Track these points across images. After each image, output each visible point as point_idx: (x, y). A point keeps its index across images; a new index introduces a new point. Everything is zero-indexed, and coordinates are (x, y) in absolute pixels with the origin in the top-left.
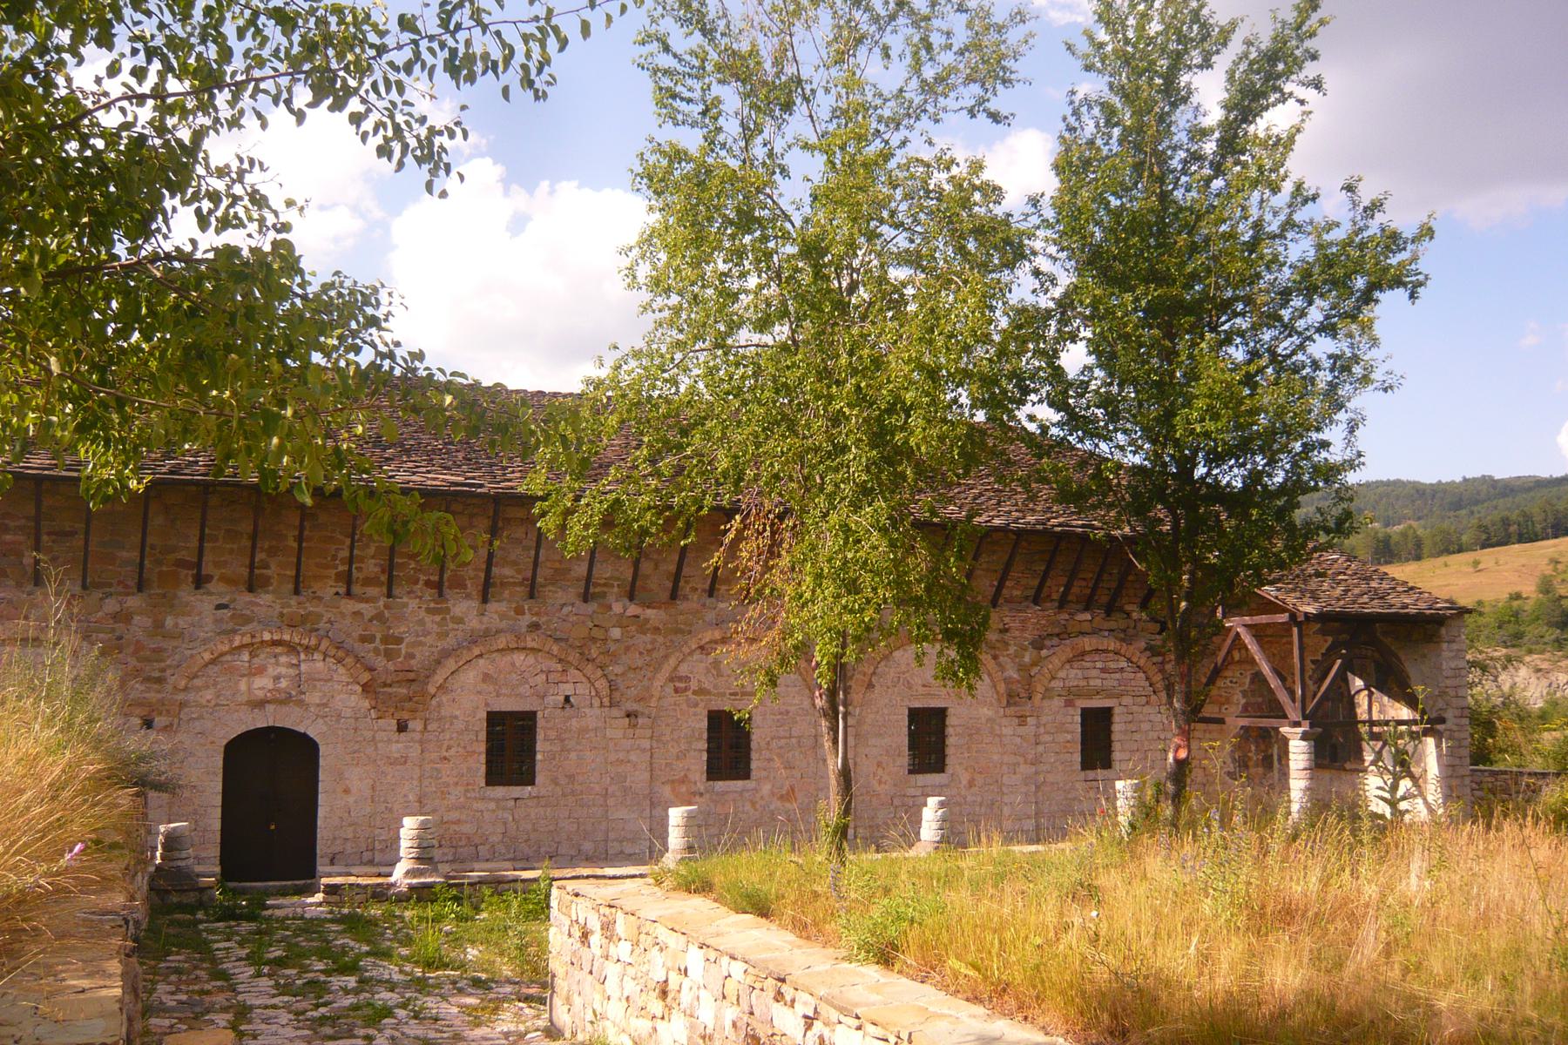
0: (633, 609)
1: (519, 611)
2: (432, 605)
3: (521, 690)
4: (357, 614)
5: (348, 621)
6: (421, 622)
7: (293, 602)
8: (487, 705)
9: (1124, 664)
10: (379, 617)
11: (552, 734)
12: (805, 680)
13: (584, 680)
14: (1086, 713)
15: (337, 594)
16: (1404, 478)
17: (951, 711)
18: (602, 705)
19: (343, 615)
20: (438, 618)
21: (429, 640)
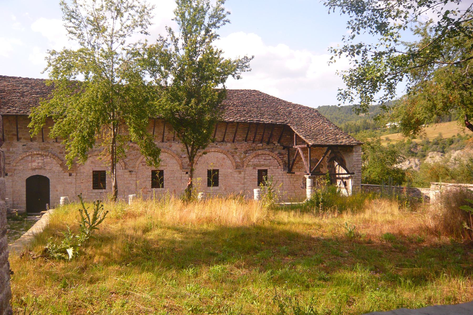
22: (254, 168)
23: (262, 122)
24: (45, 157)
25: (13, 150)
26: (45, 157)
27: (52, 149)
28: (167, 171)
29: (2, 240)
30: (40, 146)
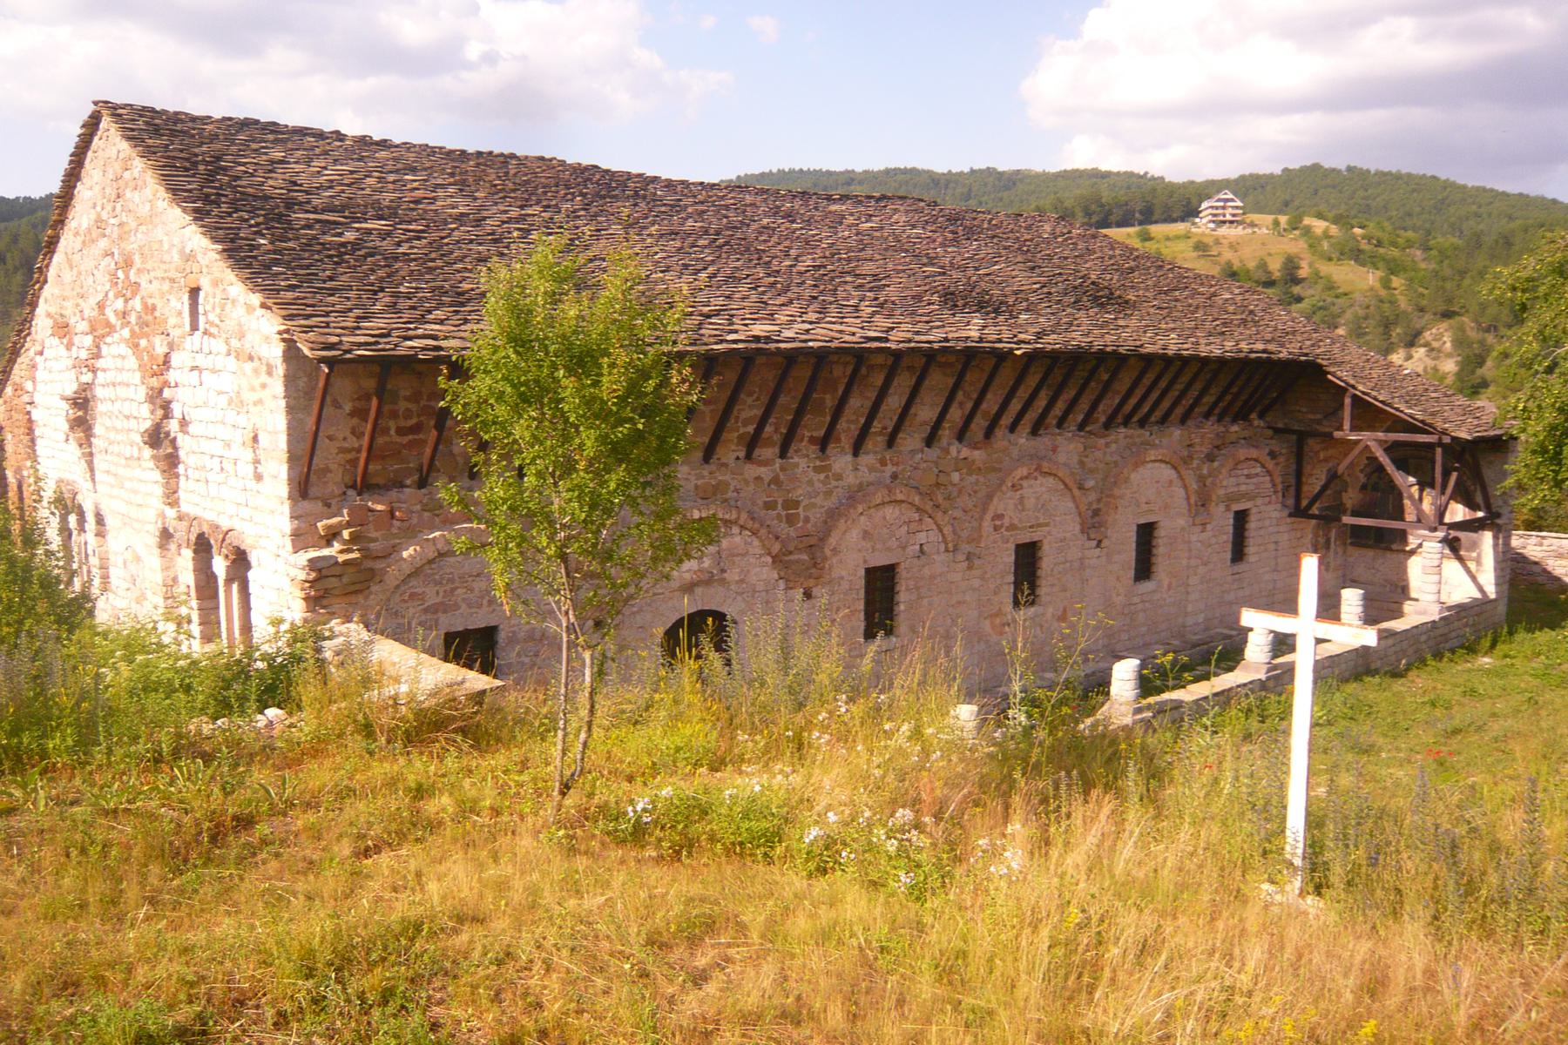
0: (965, 452)
1: (883, 463)
2: (818, 463)
3: (889, 544)
4: (758, 479)
5: (751, 487)
6: (810, 482)
7: (706, 473)
8: (865, 562)
9: (1259, 470)
10: (775, 480)
11: (911, 583)
12: (1077, 507)
13: (934, 527)
14: (1237, 513)
15: (738, 458)
16: (920, 167)
17: (1161, 524)
18: (947, 550)
19: (747, 482)
20: (822, 476)
21: (818, 500)
22: (1228, 508)
23: (961, 345)
27: (737, 491)
28: (1050, 543)
29: (49, 315)
30: (699, 483)
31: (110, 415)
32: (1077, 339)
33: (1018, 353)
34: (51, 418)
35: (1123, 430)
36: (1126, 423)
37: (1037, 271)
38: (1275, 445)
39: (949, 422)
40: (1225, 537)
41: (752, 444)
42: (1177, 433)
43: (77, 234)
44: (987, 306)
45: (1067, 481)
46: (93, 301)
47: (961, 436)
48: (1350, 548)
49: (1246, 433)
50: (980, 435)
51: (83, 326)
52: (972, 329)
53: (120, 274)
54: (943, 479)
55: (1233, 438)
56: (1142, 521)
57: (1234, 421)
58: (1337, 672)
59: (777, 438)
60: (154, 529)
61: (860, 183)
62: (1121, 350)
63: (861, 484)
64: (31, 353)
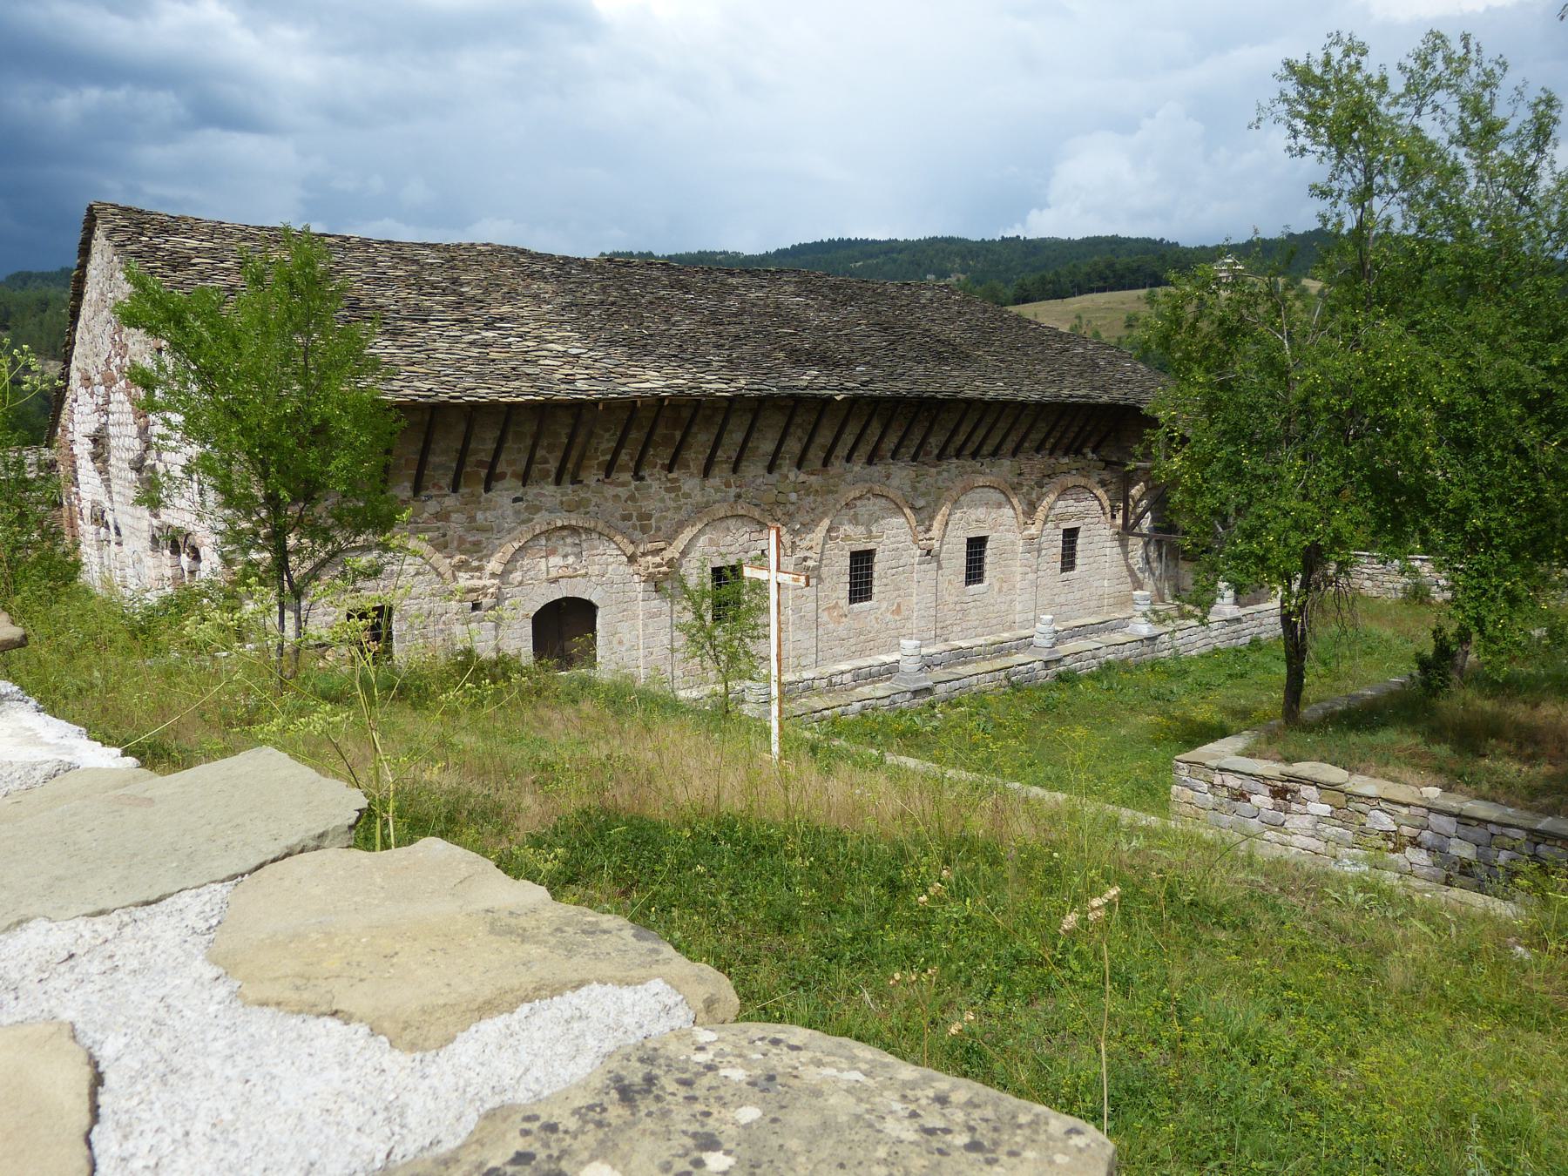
0: (802, 477)
1: (728, 485)
10: (632, 498)
20: (673, 495)
21: (669, 514)
24: (584, 537)
25: (486, 520)
26: (584, 537)
31: (118, 448)
32: (901, 387)
33: (838, 398)
34: (83, 449)
35: (954, 460)
36: (958, 455)
37: (890, 331)
38: (1106, 475)
39: (788, 453)
40: (1055, 550)
41: (609, 468)
42: (1007, 463)
43: (90, 305)
44: (825, 361)
45: (898, 501)
46: (103, 359)
47: (799, 464)
48: (1181, 562)
49: (1078, 465)
50: (818, 464)
51: (98, 379)
52: (807, 379)
53: (116, 337)
54: (781, 498)
55: (1065, 468)
56: (972, 535)
57: (1066, 454)
58: (30, 517)
59: (632, 464)
60: (147, 535)
61: (900, 252)
62: (938, 396)
63: (708, 502)
64: (70, 400)
